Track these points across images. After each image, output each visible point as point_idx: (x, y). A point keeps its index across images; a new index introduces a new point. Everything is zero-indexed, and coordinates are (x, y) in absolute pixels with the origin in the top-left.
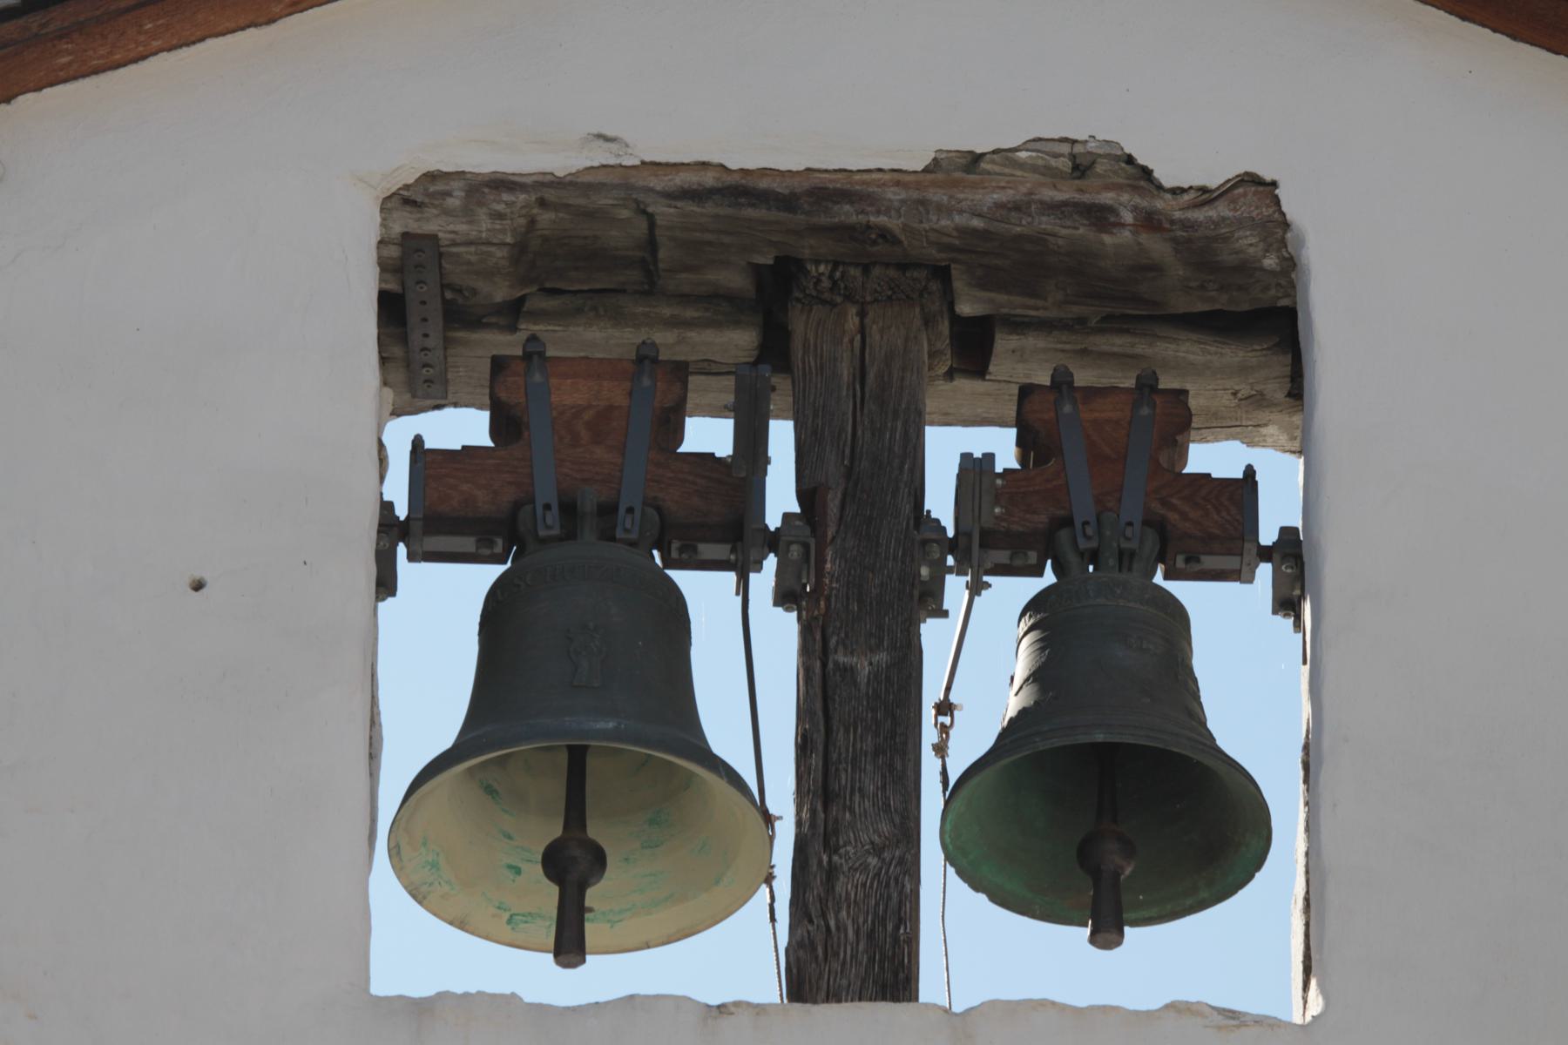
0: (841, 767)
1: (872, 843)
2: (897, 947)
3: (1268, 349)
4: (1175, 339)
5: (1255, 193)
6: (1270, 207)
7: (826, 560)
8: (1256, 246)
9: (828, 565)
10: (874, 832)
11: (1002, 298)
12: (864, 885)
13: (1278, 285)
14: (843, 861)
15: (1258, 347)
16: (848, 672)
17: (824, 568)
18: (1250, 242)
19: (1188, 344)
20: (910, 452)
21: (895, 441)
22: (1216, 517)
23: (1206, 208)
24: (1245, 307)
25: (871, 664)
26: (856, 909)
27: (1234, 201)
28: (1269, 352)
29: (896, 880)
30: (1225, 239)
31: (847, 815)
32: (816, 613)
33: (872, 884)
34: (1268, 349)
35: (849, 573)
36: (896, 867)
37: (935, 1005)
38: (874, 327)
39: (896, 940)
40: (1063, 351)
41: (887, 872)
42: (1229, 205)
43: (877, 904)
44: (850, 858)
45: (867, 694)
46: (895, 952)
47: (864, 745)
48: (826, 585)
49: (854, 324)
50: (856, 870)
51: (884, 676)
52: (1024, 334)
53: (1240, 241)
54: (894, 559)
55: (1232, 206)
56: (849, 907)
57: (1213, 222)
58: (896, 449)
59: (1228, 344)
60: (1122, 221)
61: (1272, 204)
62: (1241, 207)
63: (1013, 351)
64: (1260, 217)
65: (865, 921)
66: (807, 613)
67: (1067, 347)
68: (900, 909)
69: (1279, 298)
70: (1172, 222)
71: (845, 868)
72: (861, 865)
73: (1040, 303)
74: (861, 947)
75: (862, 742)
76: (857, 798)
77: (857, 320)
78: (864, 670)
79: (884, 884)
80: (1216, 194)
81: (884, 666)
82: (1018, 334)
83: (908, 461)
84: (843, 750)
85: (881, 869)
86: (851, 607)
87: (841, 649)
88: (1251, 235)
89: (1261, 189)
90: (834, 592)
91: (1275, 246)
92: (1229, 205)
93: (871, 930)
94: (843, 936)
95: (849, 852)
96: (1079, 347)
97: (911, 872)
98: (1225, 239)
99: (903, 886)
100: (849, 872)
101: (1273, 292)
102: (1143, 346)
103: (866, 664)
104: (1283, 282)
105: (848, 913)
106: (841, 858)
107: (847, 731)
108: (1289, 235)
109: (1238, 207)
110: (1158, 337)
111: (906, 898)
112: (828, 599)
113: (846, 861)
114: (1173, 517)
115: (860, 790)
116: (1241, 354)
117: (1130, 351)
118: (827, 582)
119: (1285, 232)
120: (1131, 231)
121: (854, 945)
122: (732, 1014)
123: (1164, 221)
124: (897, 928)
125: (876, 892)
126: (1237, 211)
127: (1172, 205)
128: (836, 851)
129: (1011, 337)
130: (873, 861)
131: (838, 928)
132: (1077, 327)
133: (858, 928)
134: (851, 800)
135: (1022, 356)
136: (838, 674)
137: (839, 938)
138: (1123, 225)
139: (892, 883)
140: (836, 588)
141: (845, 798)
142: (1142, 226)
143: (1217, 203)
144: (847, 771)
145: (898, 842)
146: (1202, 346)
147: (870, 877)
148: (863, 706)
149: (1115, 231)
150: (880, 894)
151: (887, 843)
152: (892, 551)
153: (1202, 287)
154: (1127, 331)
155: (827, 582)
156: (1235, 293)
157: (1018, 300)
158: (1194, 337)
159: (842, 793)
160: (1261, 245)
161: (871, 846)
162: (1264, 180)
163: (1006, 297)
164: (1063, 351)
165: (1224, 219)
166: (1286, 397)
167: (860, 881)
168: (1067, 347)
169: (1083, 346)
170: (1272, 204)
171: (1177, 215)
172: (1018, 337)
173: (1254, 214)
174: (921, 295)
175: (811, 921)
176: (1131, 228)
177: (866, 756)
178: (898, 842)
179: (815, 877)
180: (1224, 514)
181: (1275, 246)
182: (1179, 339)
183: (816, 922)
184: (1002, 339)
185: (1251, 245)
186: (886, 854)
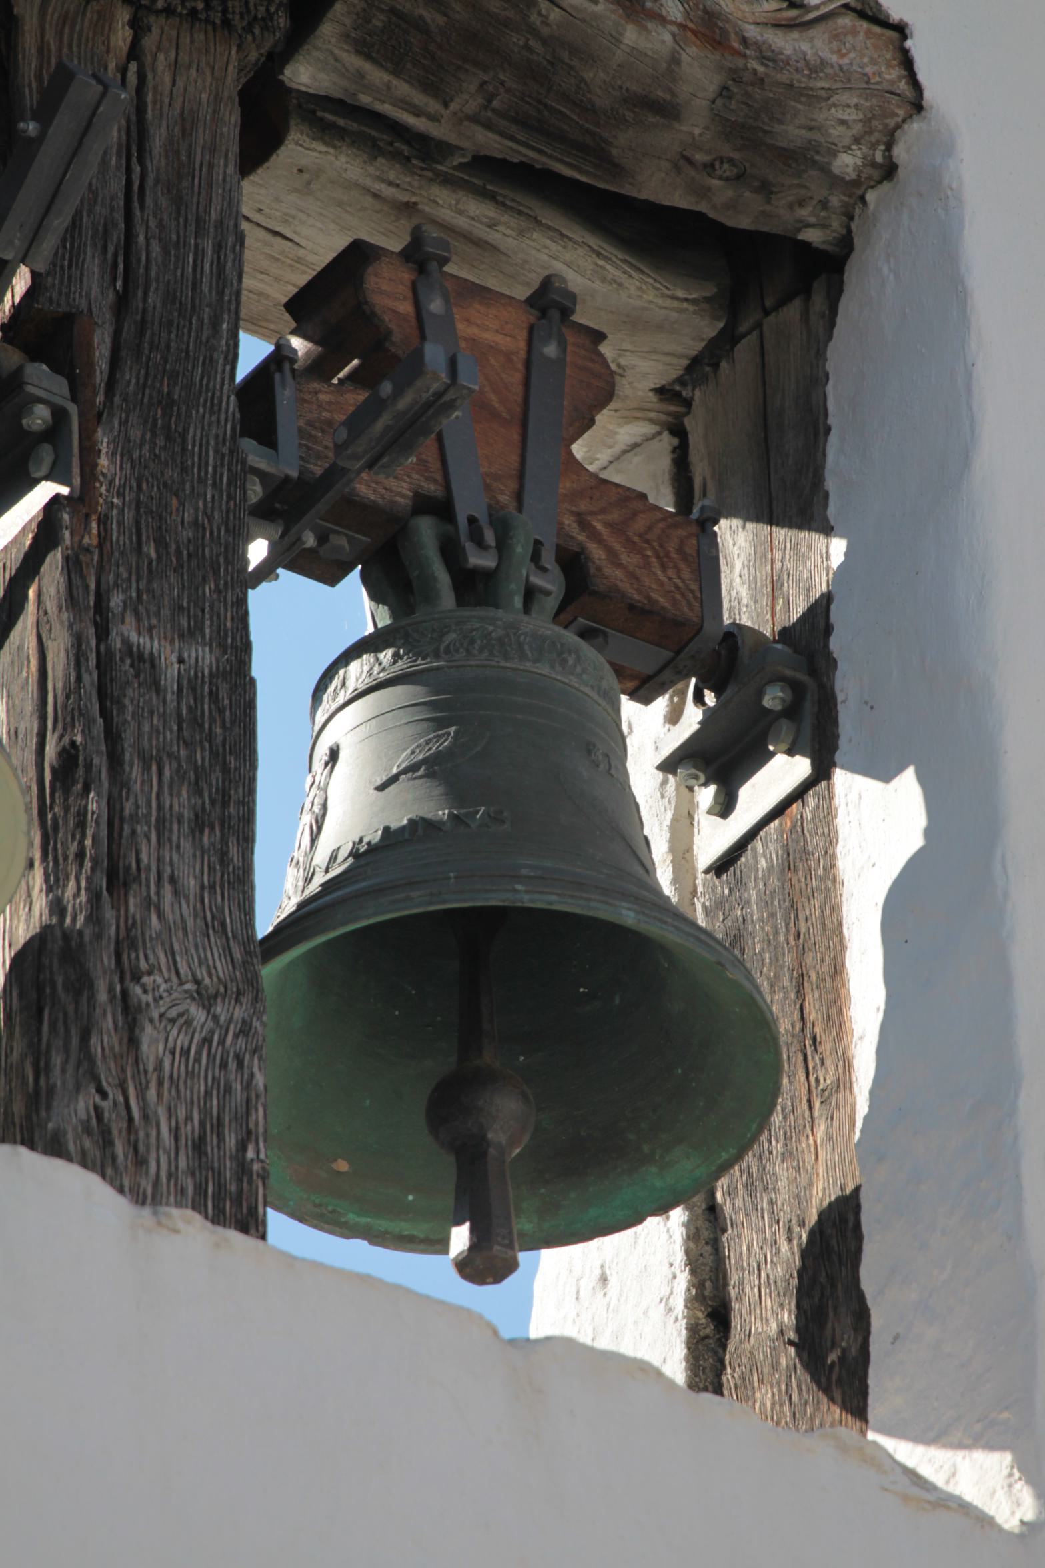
0: (139, 828)
1: (197, 982)
2: (245, 1179)
3: (694, 302)
4: (563, 235)
5: (868, 33)
6: (893, 67)
7: (100, 451)
8: (848, 127)
9: (103, 461)
10: (200, 964)
11: (377, 75)
12: (185, 1052)
13: (824, 204)
14: (150, 998)
15: (681, 294)
16: (145, 663)
17: (96, 465)
18: (846, 117)
19: (581, 251)
20: (230, 301)
21: (202, 273)
22: (660, 573)
23: (795, 34)
24: (744, 222)
25: (181, 661)
26: (173, 1092)
27: (836, 37)
28: (691, 308)
29: (240, 1064)
30: (813, 98)
31: (154, 918)
32: (86, 540)
33: (198, 1053)
34: (694, 302)
35: (139, 487)
36: (236, 1036)
37: (481, 1317)
38: (161, 57)
39: (243, 1168)
40: (376, 196)
41: (222, 1042)
42: (830, 42)
43: (208, 1094)
44: (161, 998)
45: (179, 715)
46: (242, 1190)
47: (175, 801)
48: (101, 495)
49: (124, 40)
50: (173, 1021)
51: (206, 689)
52: (334, 147)
53: (833, 110)
54: (214, 484)
55: (835, 45)
56: (160, 1084)
57: (807, 63)
58: (205, 289)
59: (643, 272)
60: (664, 13)
61: (895, 63)
62: (849, 52)
63: (300, 171)
64: (877, 79)
65: (189, 1118)
66: (72, 534)
67: (387, 191)
68: (248, 1113)
69: (809, 226)
70: (744, 41)
71: (155, 1014)
72: (181, 1015)
73: (433, 106)
74: (182, 1164)
75: (171, 795)
76: (167, 890)
77: (128, 33)
78: (171, 672)
79: (218, 1062)
80: (812, 16)
81: (206, 672)
82: (326, 144)
83: (226, 316)
84: (142, 801)
85: (212, 1032)
86: (145, 549)
87: (130, 618)
88: (857, 106)
89: (877, 29)
90: (115, 512)
91: (876, 136)
92: (830, 42)
93: (200, 1138)
94: (154, 1133)
95: (158, 987)
96: (404, 197)
97: (264, 1052)
98: (813, 98)
99: (252, 1075)
100: (160, 1022)
101: (804, 213)
102: (508, 232)
103: (174, 658)
104: (835, 201)
105: (160, 1095)
106: (145, 991)
107: (146, 768)
108: (915, 126)
109: (844, 51)
110: (538, 222)
111: (257, 1096)
112: (103, 521)
113: (155, 1000)
114: (597, 553)
115: (173, 880)
116: (650, 295)
117: (481, 232)
118: (103, 490)
119: (908, 118)
120: (674, 35)
121: (173, 1155)
122: (176, 1231)
123: (733, 36)
124: (242, 1146)
125: (206, 1070)
126: (843, 56)
127: (744, 12)
128: (137, 977)
129: (315, 145)
130: (198, 1015)
131: (145, 1117)
132: (414, 162)
133: (177, 1128)
134: (158, 893)
135: (309, 183)
136: (128, 661)
137: (147, 1135)
138: (663, 20)
139: (232, 1065)
140: (117, 506)
141: (148, 886)
142: (695, 33)
143: (812, 32)
144: (149, 840)
145: (239, 994)
146: (601, 262)
147: (195, 1041)
148: (171, 731)
149: (650, 25)
150: (213, 1078)
151: (222, 990)
152: (210, 469)
153: (709, 167)
154: (492, 197)
155: (103, 490)
156: (747, 194)
157: (402, 88)
158: (595, 242)
159: (143, 876)
160: (857, 129)
161: (195, 987)
162: (888, 16)
163: (386, 77)
164: (376, 196)
165: (823, 63)
166: (652, 390)
167: (179, 1043)
168: (387, 191)
169: (413, 199)
170: (895, 63)
171: (752, 32)
172: (323, 148)
173: (868, 70)
174: (249, 29)
175: (104, 1095)
176: (674, 29)
177: (179, 822)
178: (239, 994)
179: (105, 1012)
180: (671, 573)
181: (876, 136)
182: (570, 239)
183: (111, 1096)
184: (297, 144)
185: (843, 122)
186: (219, 1009)
